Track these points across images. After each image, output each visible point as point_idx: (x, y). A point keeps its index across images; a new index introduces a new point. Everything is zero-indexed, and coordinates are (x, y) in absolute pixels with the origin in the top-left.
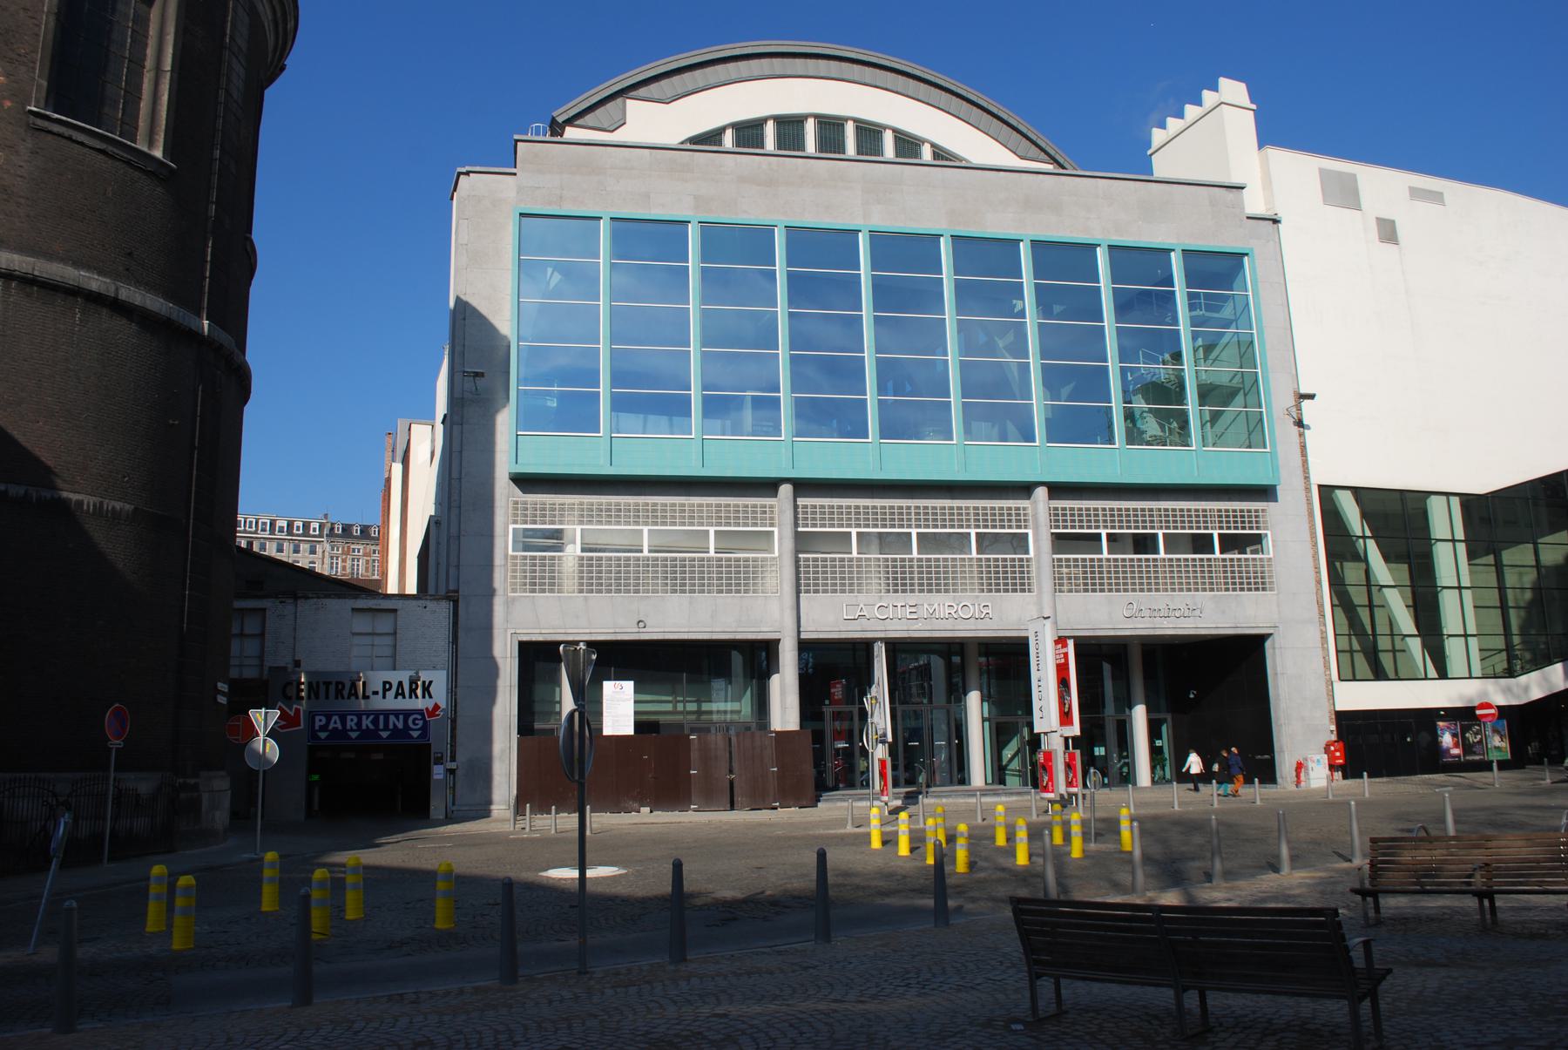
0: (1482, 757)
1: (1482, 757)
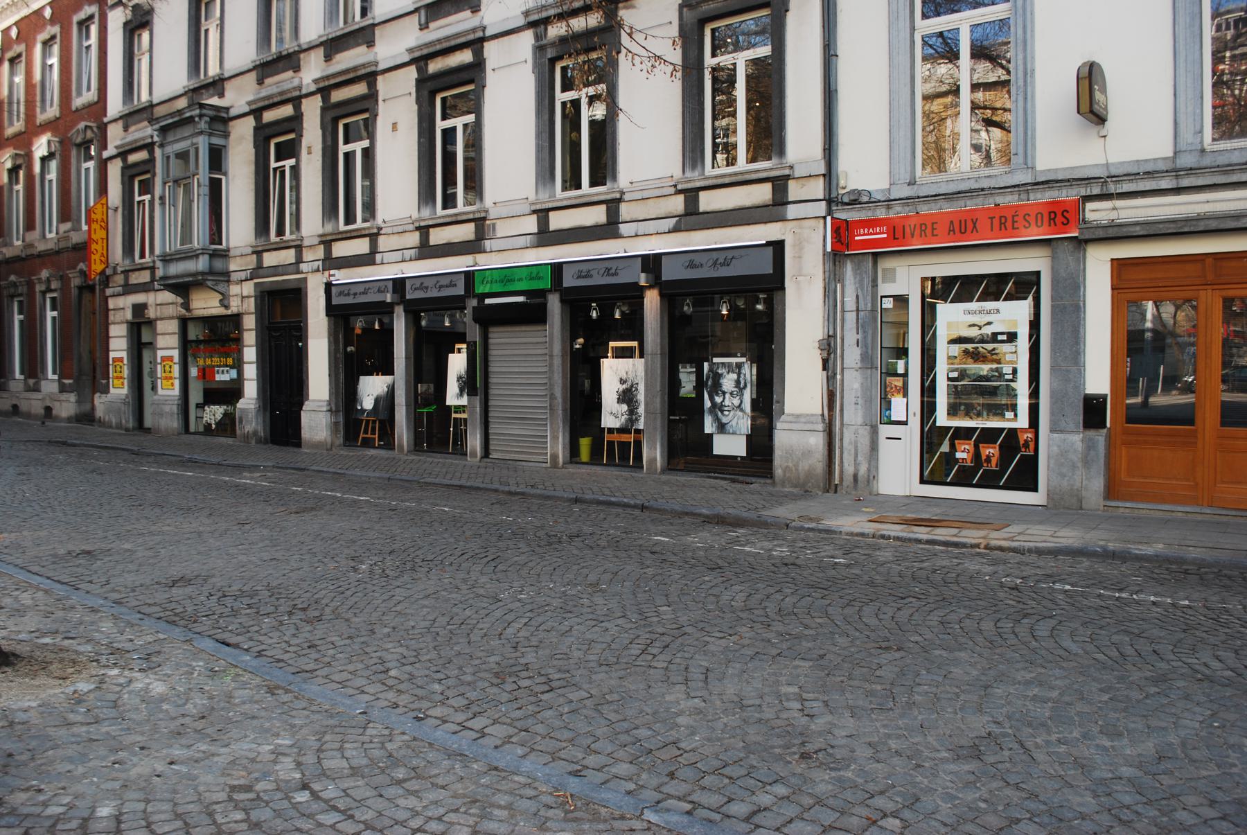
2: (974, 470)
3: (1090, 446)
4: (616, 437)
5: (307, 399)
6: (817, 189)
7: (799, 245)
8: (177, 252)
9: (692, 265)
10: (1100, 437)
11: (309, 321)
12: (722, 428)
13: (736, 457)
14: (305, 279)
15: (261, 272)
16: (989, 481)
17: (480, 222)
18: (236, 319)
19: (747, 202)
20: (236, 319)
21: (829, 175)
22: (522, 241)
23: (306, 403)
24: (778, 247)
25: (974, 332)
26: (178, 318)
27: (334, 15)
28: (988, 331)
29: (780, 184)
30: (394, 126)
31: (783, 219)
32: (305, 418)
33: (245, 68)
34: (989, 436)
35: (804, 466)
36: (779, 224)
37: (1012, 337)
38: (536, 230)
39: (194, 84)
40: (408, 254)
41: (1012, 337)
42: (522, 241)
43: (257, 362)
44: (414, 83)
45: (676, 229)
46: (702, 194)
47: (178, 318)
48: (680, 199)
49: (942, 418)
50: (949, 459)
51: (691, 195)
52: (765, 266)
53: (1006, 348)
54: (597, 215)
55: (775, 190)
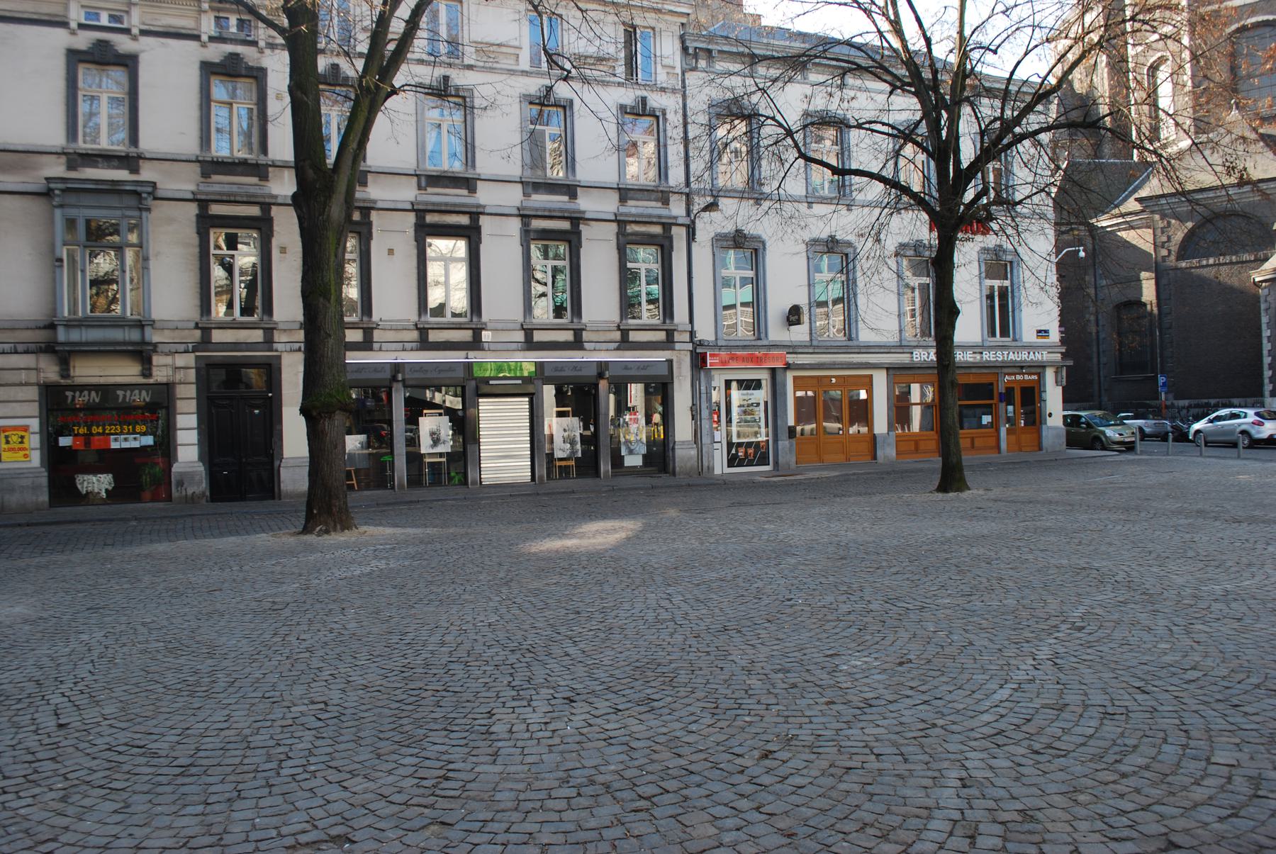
0: (1050, 375)
1: (1050, 375)
2: (744, 459)
3: (791, 446)
4: (563, 463)
5: (176, 460)
6: (686, 337)
7: (679, 363)
8: (86, 319)
9: (626, 368)
10: (794, 441)
11: (284, 392)
12: (631, 452)
13: (636, 467)
14: (279, 357)
15: (210, 346)
16: (750, 464)
17: (578, 333)
18: (167, 390)
19: (654, 339)
20: (167, 390)
21: (692, 333)
22: (514, 346)
23: (175, 465)
24: (670, 362)
25: (745, 403)
26: (38, 384)
27: (570, 169)
28: (750, 402)
29: (670, 333)
30: (391, 252)
31: (673, 349)
32: (284, 474)
33: (53, 150)
34: (749, 445)
35: (689, 465)
36: (670, 352)
37: (758, 404)
38: (523, 340)
39: (529, 176)
40: (408, 346)
41: (758, 404)
42: (514, 346)
43: (175, 429)
44: (194, 219)
45: (618, 349)
46: (213, 331)
47: (38, 384)
48: (198, 333)
49: (735, 440)
50: (736, 456)
51: (206, 331)
52: (665, 372)
53: (757, 409)
54: (568, 336)
55: (667, 335)
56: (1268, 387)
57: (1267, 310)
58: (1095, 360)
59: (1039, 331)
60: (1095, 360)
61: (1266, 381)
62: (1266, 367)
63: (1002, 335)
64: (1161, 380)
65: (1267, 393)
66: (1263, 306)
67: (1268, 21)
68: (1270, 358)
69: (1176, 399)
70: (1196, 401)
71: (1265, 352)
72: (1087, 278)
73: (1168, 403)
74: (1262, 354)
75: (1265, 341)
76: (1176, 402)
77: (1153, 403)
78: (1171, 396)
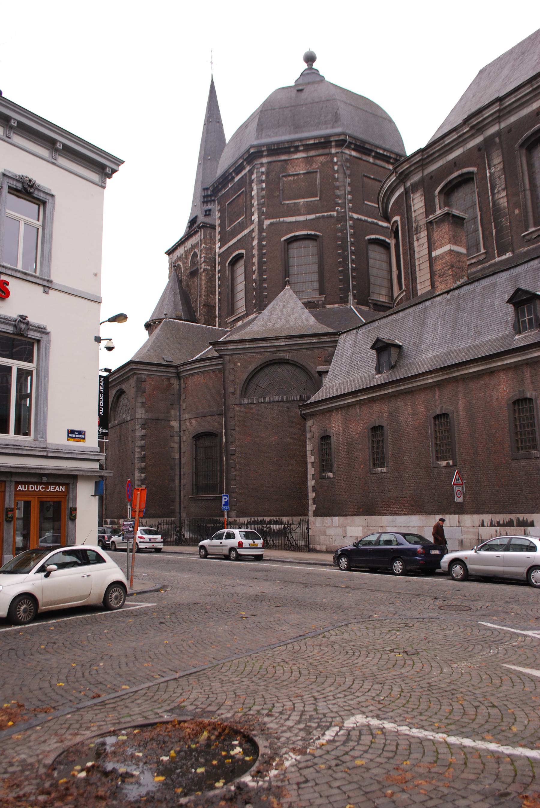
56: (312, 508)
57: (312, 438)
58: (177, 482)
59: (71, 432)
60: (177, 482)
61: (310, 502)
62: (310, 489)
63: (18, 432)
64: (225, 499)
65: (311, 513)
66: (308, 436)
67: (311, 235)
68: (313, 482)
69: (237, 517)
70: (254, 519)
71: (310, 477)
72: (173, 412)
73: (232, 520)
74: (307, 478)
75: (309, 466)
76: (238, 519)
77: (221, 519)
78: (233, 513)
